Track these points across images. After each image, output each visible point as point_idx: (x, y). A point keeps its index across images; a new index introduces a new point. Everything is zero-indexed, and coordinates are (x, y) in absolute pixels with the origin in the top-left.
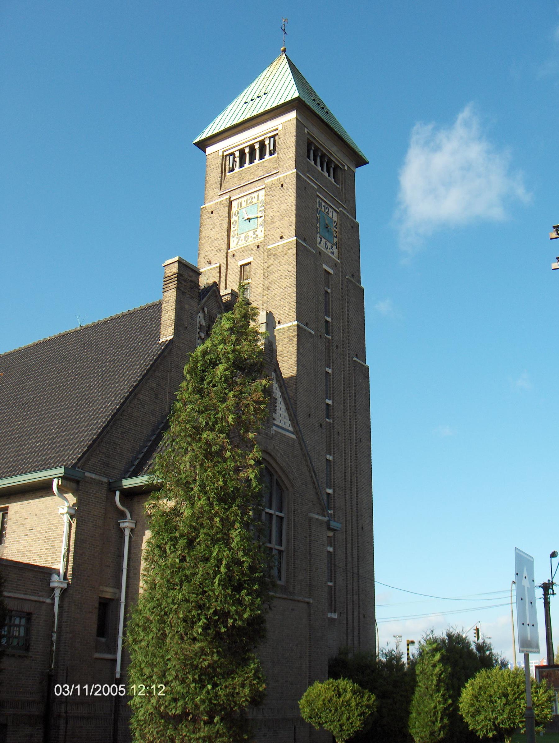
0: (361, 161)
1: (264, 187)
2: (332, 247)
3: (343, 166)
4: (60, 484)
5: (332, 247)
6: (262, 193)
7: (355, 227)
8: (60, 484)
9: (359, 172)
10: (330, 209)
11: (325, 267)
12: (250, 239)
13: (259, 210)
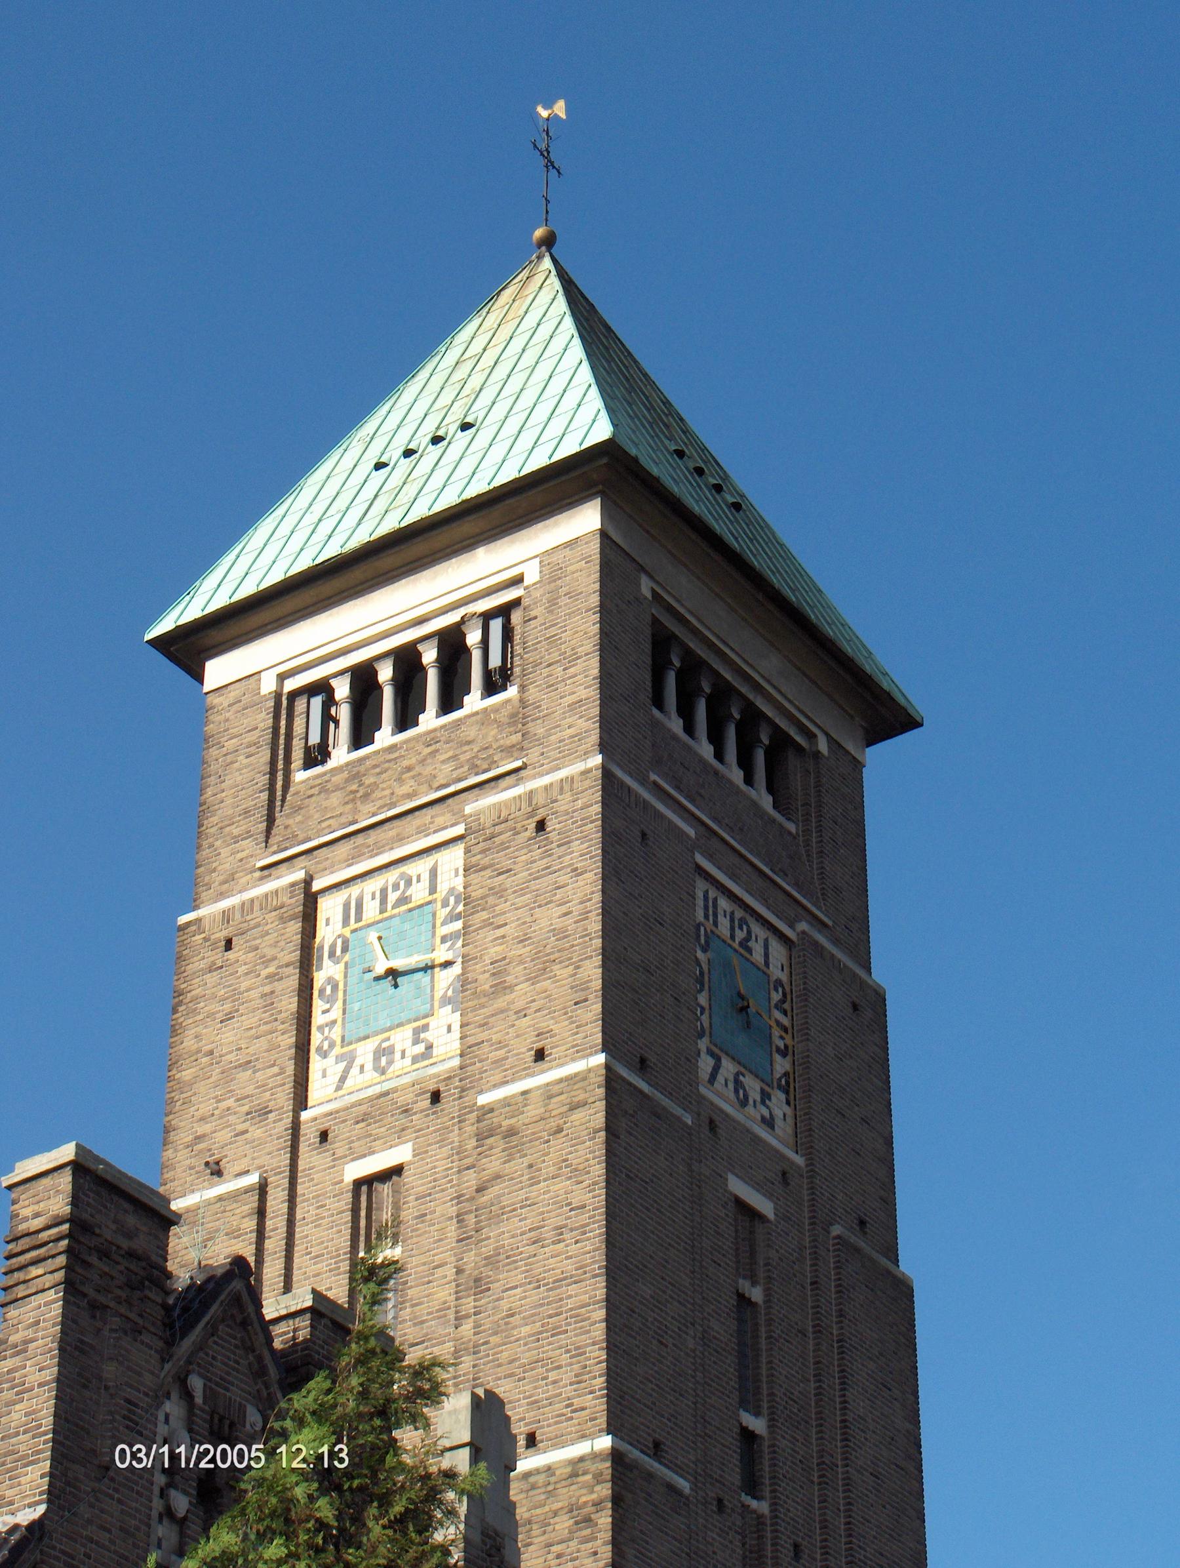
0: (888, 717)
1: (459, 830)
2: (765, 1096)
3: (811, 736)
5: (765, 1096)
6: (453, 858)
9: (882, 763)
13: (442, 931)
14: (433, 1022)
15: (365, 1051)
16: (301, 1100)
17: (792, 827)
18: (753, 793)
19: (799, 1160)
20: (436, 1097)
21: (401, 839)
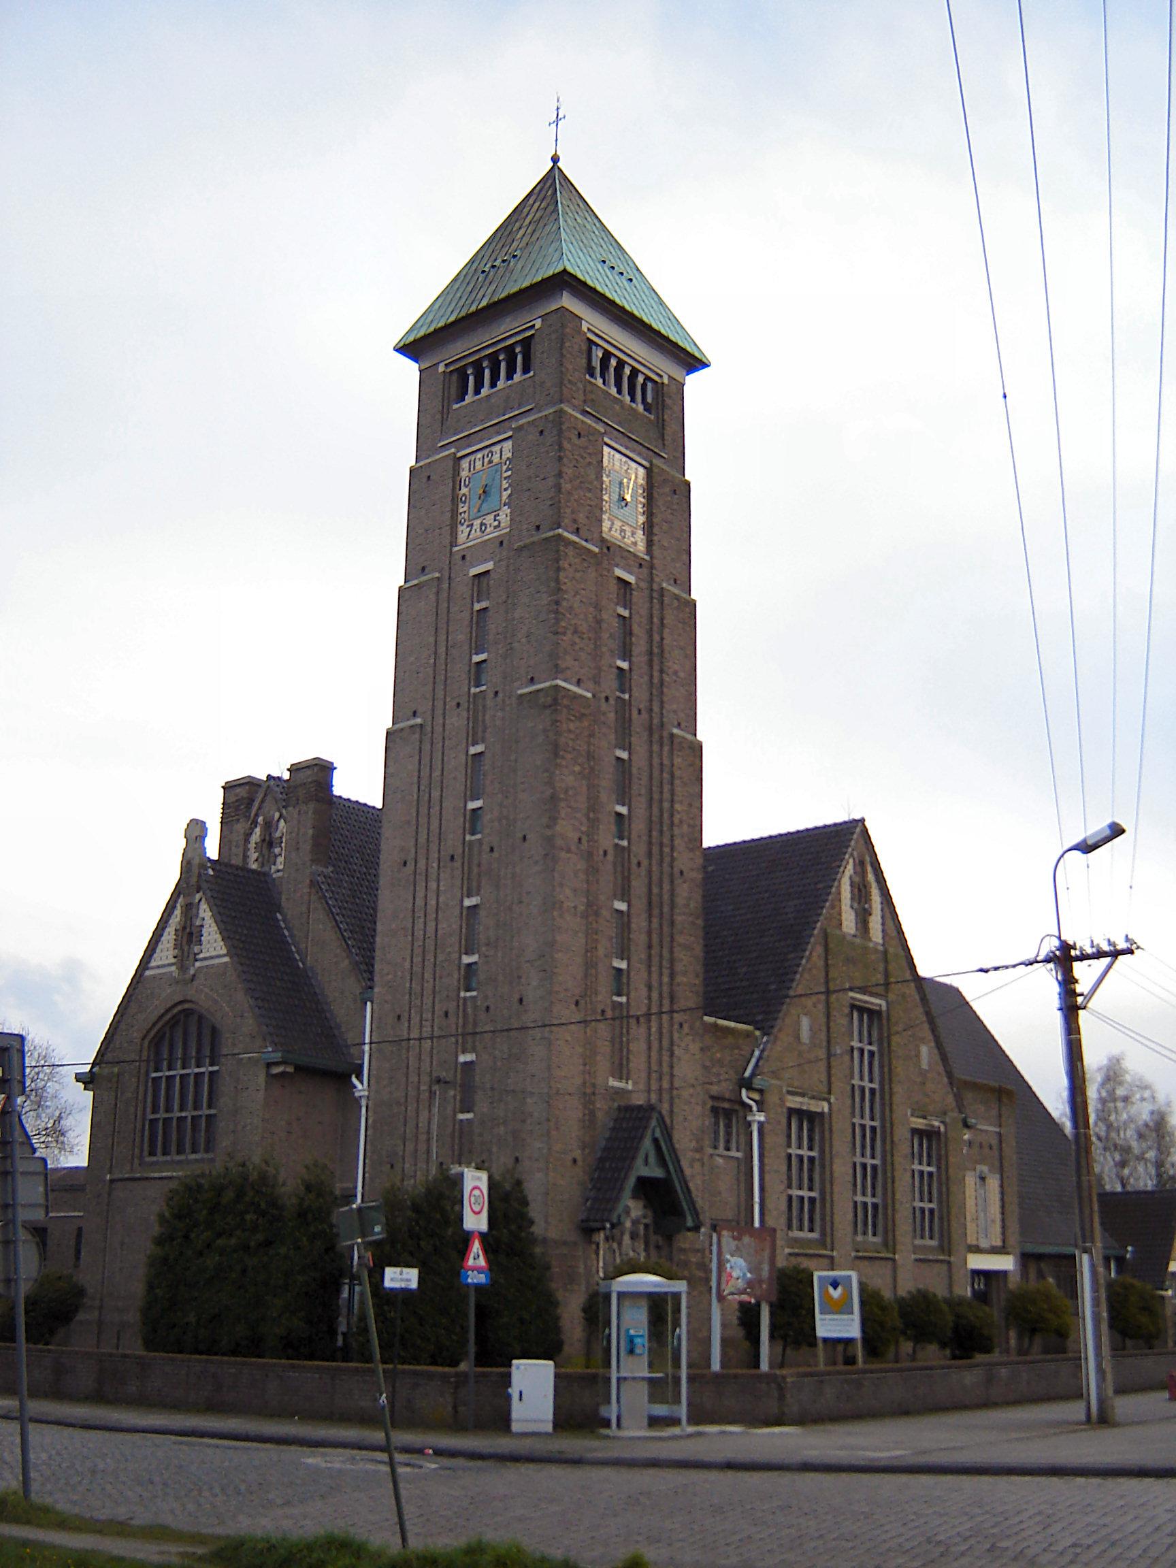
0: (694, 363)
1: (510, 434)
2: (633, 534)
3: (661, 376)
4: (624, 474)
5: (633, 534)
6: (508, 445)
7: (684, 490)
8: (624, 474)
9: (693, 383)
10: (633, 465)
11: (619, 572)
12: (488, 530)
13: (505, 475)
14: (501, 513)
15: (477, 523)
16: (453, 543)
17: (652, 417)
18: (634, 405)
19: (647, 558)
20: (501, 543)
21: (633, 451)
